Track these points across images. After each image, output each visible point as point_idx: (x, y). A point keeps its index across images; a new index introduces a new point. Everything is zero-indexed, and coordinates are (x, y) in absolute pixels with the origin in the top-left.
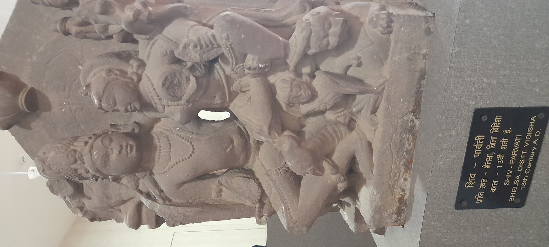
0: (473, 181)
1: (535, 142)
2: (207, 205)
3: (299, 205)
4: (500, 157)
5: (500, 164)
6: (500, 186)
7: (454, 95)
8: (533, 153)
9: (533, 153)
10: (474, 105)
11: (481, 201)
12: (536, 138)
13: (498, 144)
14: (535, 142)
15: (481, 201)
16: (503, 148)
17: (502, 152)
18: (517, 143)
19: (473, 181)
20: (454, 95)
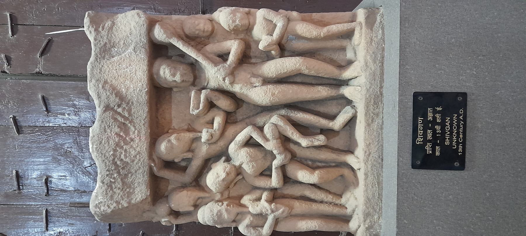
0: (421, 138)
1: (461, 117)
2: (77, 77)
3: (8, 72)
4: (438, 128)
5: (439, 133)
6: (425, 116)
7: (491, 221)
8: (461, 126)
9: (461, 126)
10: (414, 91)
11: (431, 152)
12: (461, 115)
13: (434, 118)
14: (461, 117)
15: (431, 152)
16: (438, 121)
17: (438, 124)
18: (447, 124)
19: (421, 138)
20: (491, 221)
